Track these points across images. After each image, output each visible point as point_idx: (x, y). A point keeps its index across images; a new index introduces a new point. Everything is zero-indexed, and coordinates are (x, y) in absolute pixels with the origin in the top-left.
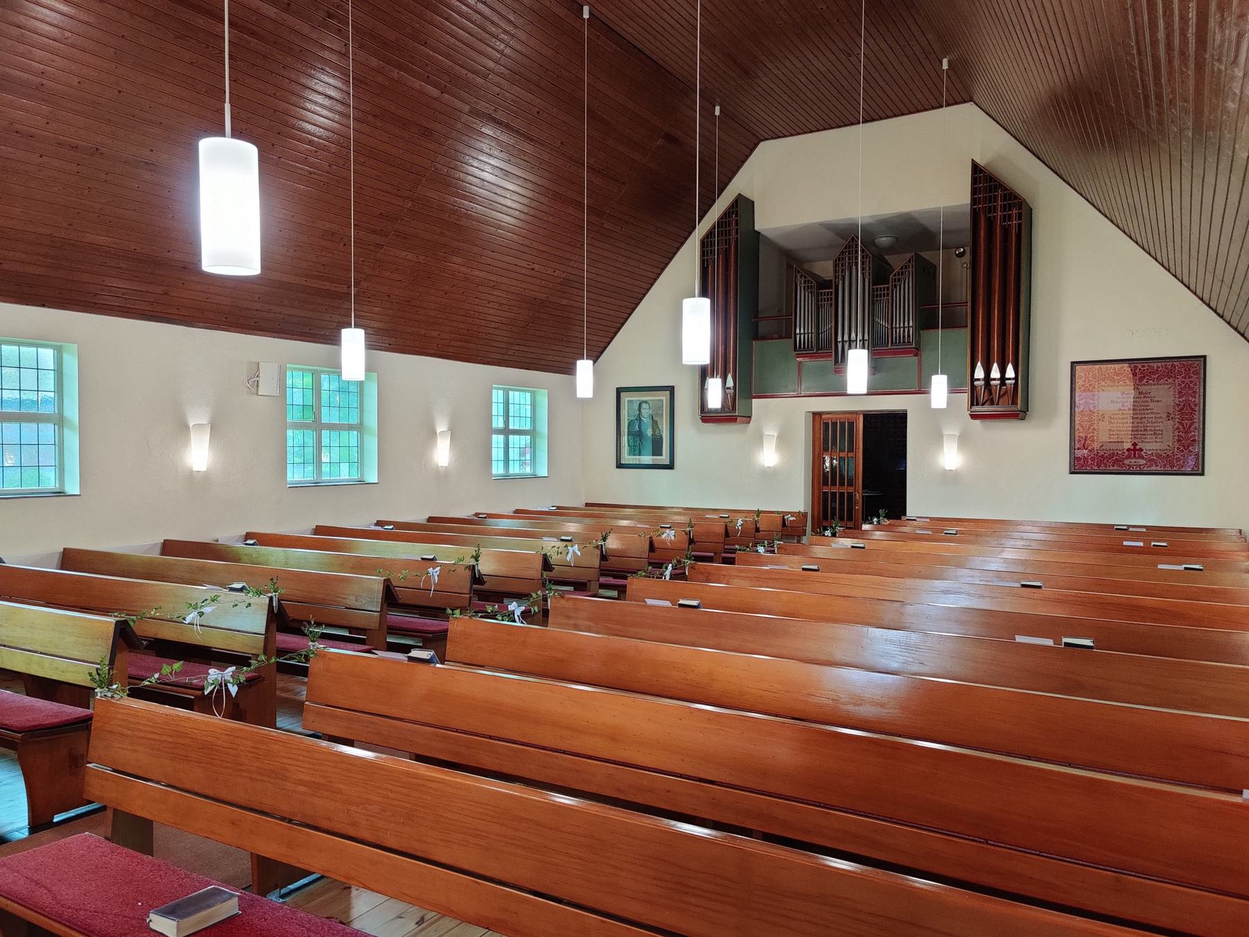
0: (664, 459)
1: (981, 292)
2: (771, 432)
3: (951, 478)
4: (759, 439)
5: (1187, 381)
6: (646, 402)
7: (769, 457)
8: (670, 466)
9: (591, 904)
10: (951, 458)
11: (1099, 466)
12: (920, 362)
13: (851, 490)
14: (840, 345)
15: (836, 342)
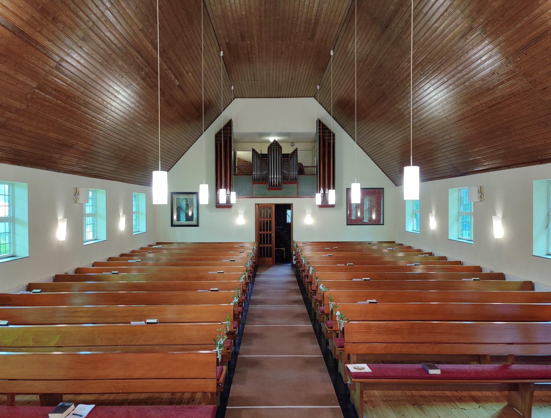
0: (194, 222)
3: (308, 229)
4: (237, 214)
8: (197, 226)
9: (24, 392)
12: (297, 186)
13: (270, 232)
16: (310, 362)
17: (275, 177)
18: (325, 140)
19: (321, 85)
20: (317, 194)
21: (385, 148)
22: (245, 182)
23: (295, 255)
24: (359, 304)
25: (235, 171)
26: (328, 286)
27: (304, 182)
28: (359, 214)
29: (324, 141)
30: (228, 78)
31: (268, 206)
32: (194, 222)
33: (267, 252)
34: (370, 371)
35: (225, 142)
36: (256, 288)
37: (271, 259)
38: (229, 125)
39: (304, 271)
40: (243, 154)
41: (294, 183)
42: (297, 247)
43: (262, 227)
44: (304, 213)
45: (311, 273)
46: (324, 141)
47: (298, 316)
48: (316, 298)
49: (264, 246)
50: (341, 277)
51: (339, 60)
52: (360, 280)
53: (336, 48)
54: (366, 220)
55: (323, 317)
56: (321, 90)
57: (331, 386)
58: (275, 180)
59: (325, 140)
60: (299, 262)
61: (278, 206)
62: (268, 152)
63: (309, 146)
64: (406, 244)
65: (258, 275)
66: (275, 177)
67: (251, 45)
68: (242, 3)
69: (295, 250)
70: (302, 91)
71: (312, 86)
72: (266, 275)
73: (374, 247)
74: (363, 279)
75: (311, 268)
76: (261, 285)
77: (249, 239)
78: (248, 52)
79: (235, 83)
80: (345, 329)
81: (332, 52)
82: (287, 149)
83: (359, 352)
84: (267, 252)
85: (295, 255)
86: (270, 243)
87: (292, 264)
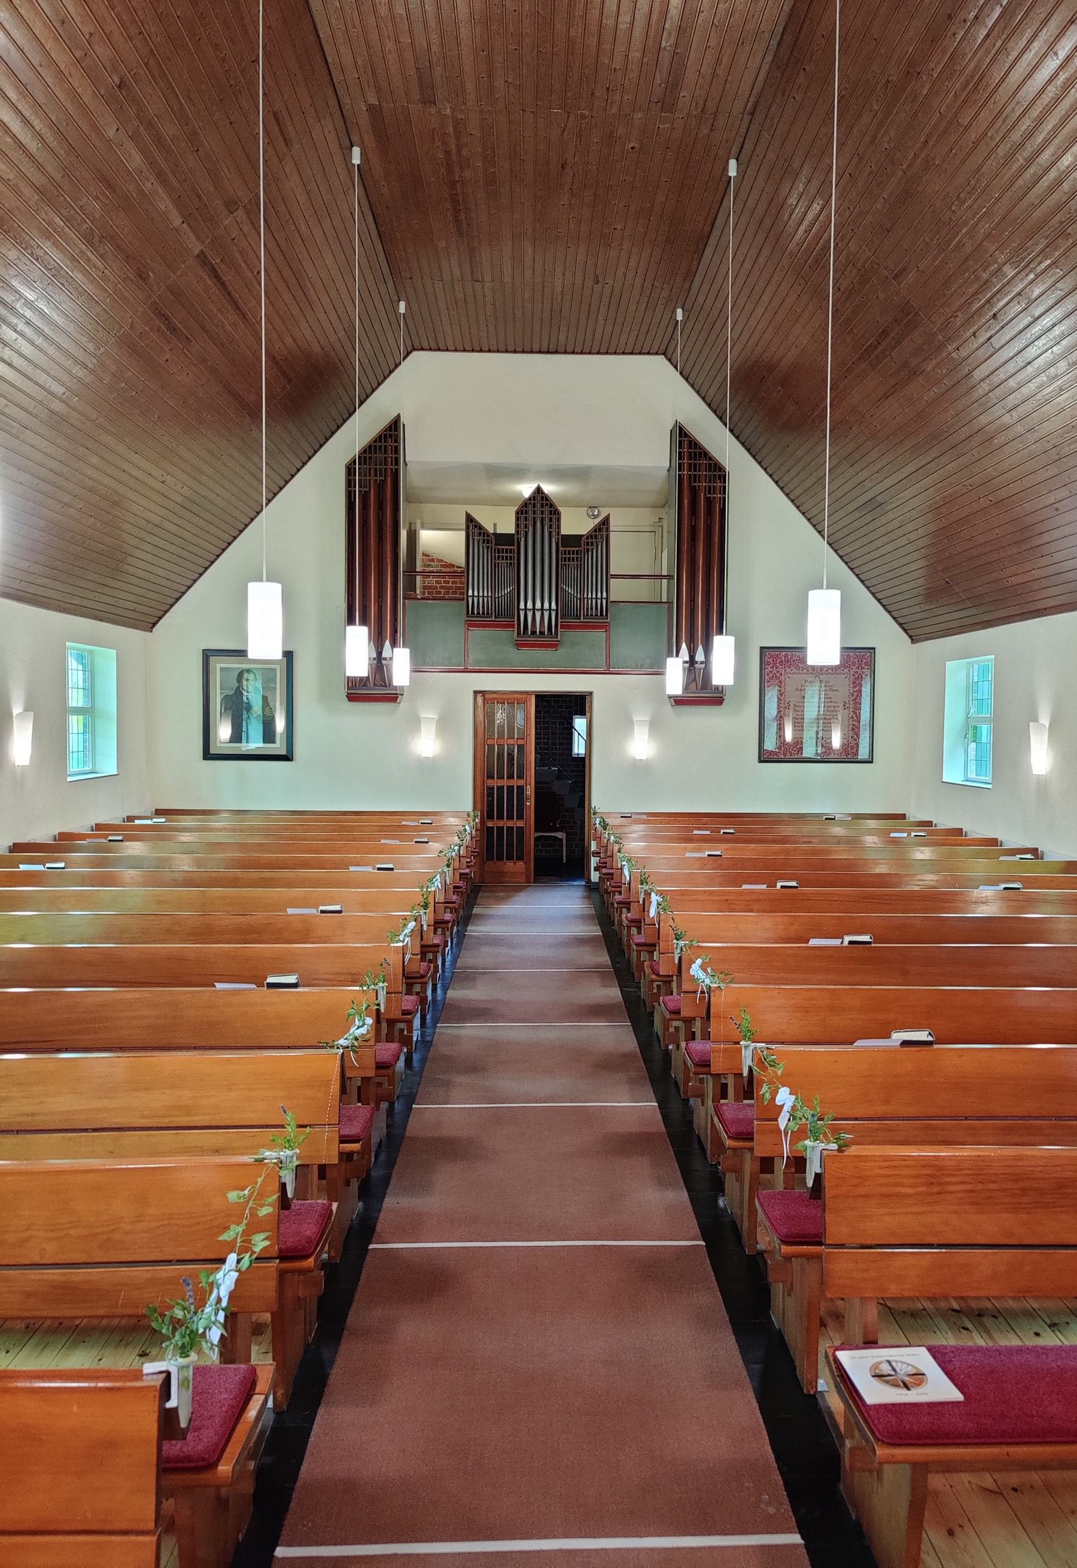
0: (278, 747)
1: (685, 556)
2: (429, 715)
3: (640, 769)
4: (414, 724)
5: (860, 671)
6: (248, 671)
7: (427, 744)
8: (287, 758)
10: (641, 746)
11: (785, 754)
12: (608, 639)
14: (522, 614)
15: (519, 609)
16: (651, 1273)
17: (538, 606)
18: (698, 497)
19: (687, 306)
20: (670, 660)
21: (890, 516)
22: (444, 625)
23: (597, 854)
24: (867, 1050)
25: (411, 586)
26: (717, 963)
27: (628, 641)
28: (789, 736)
29: (694, 492)
30: (386, 270)
31: (512, 699)
32: (277, 745)
33: (510, 845)
34: (956, 1395)
35: (377, 490)
36: (468, 959)
37: (521, 864)
38: (392, 433)
39: (627, 905)
40: (440, 541)
41: (601, 627)
42: (605, 826)
43: (492, 766)
44: (626, 725)
45: (652, 912)
46: (694, 492)
47: (607, 1065)
48: (671, 1005)
49: (501, 823)
50: (758, 930)
51: (755, 194)
52: (836, 942)
53: (748, 146)
54: (809, 751)
55: (701, 1081)
56: (689, 325)
57: (745, 1407)
58: (538, 615)
59: (698, 497)
60: (610, 874)
61: (544, 700)
62: (517, 526)
63: (644, 518)
64: (945, 821)
65: (479, 916)
66: (538, 605)
67: (456, 123)
68: (430, 8)
69: (598, 839)
70: (626, 329)
71: (660, 308)
72: (503, 917)
73: (838, 831)
74: (847, 939)
75: (654, 898)
76: (485, 949)
77: (457, 802)
78: (448, 153)
79: (410, 290)
80: (827, 1183)
81: (733, 164)
82: (575, 523)
83: (893, 1289)
84: (510, 845)
85: (597, 854)
86: (520, 817)
87: (589, 879)
